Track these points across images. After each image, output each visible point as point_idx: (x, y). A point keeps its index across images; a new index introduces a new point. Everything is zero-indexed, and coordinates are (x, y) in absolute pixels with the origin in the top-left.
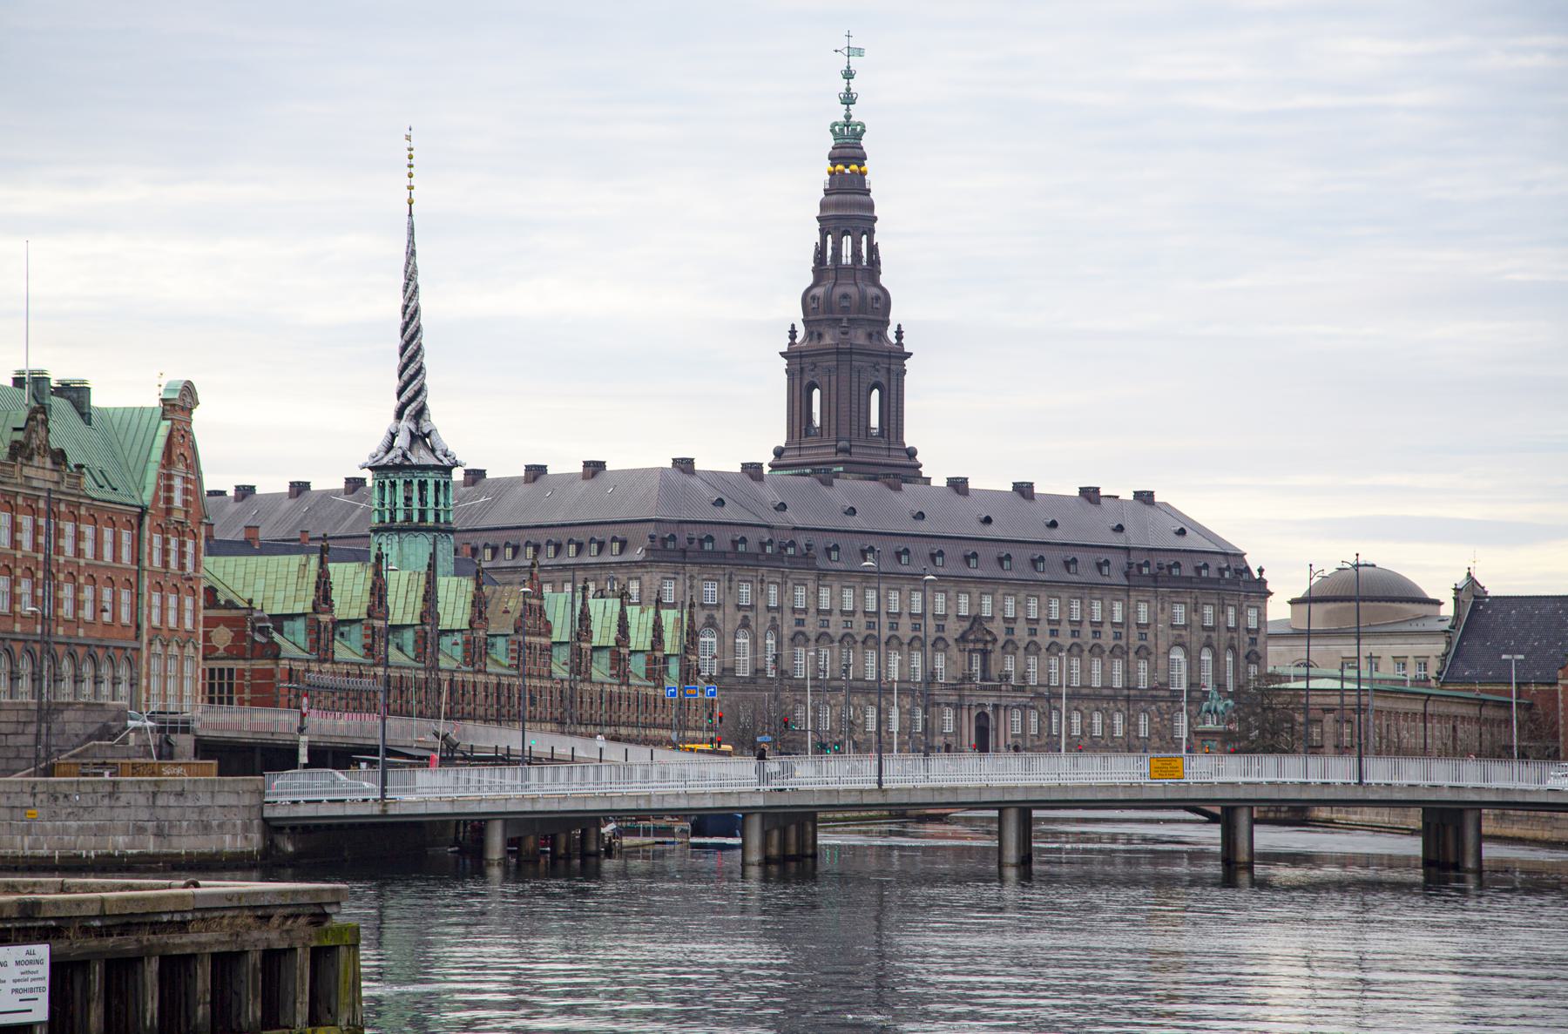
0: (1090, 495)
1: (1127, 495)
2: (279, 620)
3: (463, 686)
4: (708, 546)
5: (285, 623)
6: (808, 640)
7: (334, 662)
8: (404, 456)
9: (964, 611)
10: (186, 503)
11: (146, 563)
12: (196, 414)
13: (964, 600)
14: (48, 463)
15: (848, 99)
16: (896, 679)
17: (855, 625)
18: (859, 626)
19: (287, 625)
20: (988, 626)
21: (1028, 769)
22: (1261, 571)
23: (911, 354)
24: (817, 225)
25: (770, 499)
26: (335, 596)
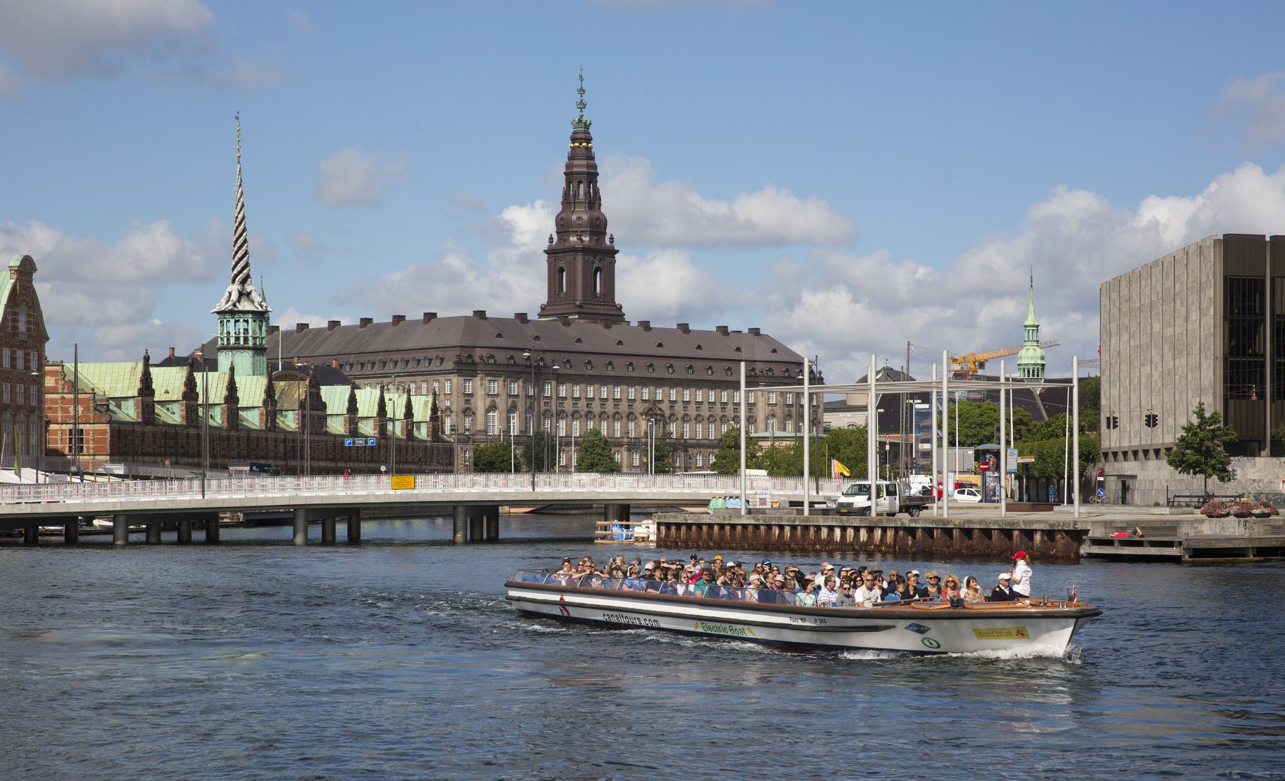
2: (118, 401)
4: (492, 361)
5: (122, 403)
7: (153, 425)
8: (234, 305)
9: (646, 397)
10: (29, 330)
13: (646, 391)
15: (582, 106)
18: (624, 407)
19: (124, 404)
22: (820, 373)
24: (564, 177)
26: (240, 394)
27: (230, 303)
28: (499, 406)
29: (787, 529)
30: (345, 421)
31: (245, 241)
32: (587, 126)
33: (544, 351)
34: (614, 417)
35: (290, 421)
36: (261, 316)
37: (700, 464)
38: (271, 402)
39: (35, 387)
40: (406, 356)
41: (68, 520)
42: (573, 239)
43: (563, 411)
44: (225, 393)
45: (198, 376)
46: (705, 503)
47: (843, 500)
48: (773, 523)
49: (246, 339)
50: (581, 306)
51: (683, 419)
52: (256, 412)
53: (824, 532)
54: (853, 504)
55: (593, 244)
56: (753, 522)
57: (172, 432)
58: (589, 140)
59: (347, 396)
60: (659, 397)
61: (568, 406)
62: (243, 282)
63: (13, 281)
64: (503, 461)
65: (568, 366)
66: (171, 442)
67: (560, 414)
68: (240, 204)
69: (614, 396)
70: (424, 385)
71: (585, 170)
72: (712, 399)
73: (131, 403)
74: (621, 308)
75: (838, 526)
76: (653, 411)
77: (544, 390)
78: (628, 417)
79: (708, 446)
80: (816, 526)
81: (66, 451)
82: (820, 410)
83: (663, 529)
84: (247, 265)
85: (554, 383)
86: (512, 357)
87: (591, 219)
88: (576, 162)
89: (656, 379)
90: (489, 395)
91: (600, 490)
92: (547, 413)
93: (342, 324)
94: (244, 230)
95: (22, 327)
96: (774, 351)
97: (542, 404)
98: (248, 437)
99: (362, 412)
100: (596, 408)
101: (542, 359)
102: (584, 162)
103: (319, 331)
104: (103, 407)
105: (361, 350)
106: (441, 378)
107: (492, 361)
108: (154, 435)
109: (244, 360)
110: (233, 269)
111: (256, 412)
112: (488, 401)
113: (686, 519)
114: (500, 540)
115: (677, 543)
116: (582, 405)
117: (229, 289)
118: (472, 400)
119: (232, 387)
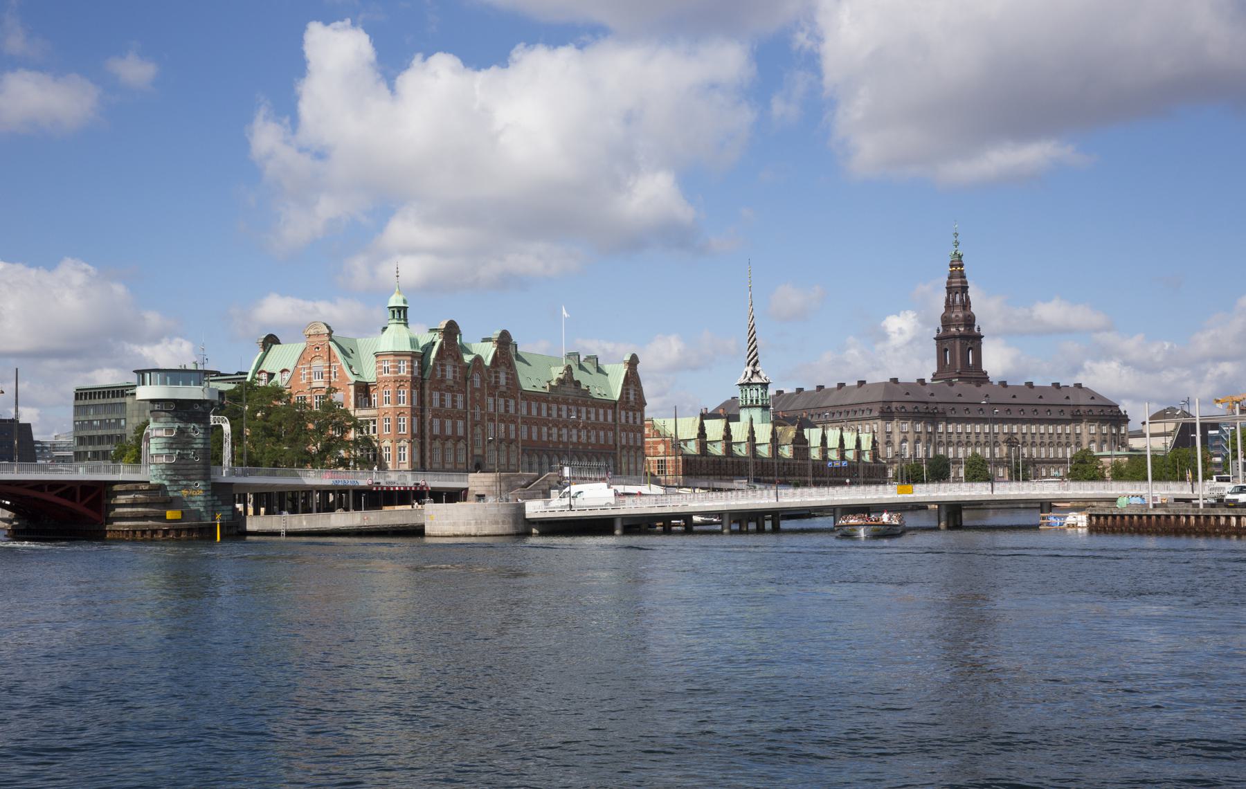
0: (1057, 385)
1: (1072, 385)
2: (686, 441)
3: (768, 464)
4: (903, 410)
6: (944, 444)
8: (749, 380)
9: (1006, 431)
10: (635, 399)
11: (618, 421)
12: (638, 366)
14: (573, 386)
15: (957, 244)
16: (674, 458)
17: (962, 437)
18: (982, 439)
19: (689, 443)
20: (1015, 436)
21: (1182, 489)
22: (1125, 412)
23: (280, 344)
24: (946, 290)
25: (927, 392)
26: (732, 433)
27: (747, 378)
28: (909, 439)
29: (1192, 518)
30: (819, 451)
31: (755, 340)
32: (960, 257)
33: (937, 403)
34: (985, 444)
35: (787, 452)
36: (765, 386)
37: (1044, 474)
38: (775, 441)
39: (640, 435)
40: (847, 409)
41: (687, 517)
42: (953, 330)
43: (951, 442)
44: (747, 435)
45: (779, 429)
46: (1114, 500)
47: (1229, 497)
48: (1181, 514)
49: (757, 401)
50: (959, 373)
51: (1031, 444)
52: (766, 447)
53: (1223, 521)
54: (1237, 500)
55: (966, 332)
56: (1165, 513)
57: (717, 461)
58: (961, 266)
59: (820, 435)
60: (1015, 431)
61: (954, 438)
62: (755, 365)
63: (626, 369)
64: (917, 475)
65: (953, 412)
66: (717, 467)
67: (949, 444)
68: (751, 316)
69: (984, 430)
70: (867, 427)
71: (960, 285)
72: (1051, 431)
73: (693, 443)
74: (986, 373)
75: (1234, 516)
76: (1011, 441)
77: (938, 428)
78: (994, 444)
79: (1049, 463)
80: (1216, 516)
81: (656, 474)
82: (1126, 437)
83: (1094, 519)
84: (756, 354)
85: (944, 423)
86: (916, 408)
87: (964, 316)
88: (953, 280)
89: (1039, 419)
90: (902, 432)
91: (1033, 493)
92: (940, 444)
93: (805, 390)
94: (754, 333)
95: (632, 398)
96: (1093, 398)
97: (937, 437)
98: (762, 463)
99: (830, 445)
100: (973, 439)
101: (936, 408)
102: (959, 280)
103: (790, 395)
104: (676, 445)
105: (818, 406)
106: (871, 422)
107: (903, 410)
108: (707, 463)
109: (757, 413)
110: (748, 357)
111: (766, 446)
112: (902, 436)
113: (1111, 511)
114: (964, 526)
115: (1105, 528)
116: (963, 437)
117: (746, 370)
118: (891, 436)
119: (752, 431)
